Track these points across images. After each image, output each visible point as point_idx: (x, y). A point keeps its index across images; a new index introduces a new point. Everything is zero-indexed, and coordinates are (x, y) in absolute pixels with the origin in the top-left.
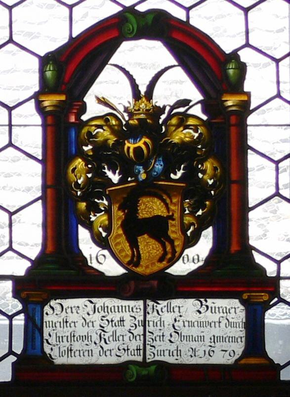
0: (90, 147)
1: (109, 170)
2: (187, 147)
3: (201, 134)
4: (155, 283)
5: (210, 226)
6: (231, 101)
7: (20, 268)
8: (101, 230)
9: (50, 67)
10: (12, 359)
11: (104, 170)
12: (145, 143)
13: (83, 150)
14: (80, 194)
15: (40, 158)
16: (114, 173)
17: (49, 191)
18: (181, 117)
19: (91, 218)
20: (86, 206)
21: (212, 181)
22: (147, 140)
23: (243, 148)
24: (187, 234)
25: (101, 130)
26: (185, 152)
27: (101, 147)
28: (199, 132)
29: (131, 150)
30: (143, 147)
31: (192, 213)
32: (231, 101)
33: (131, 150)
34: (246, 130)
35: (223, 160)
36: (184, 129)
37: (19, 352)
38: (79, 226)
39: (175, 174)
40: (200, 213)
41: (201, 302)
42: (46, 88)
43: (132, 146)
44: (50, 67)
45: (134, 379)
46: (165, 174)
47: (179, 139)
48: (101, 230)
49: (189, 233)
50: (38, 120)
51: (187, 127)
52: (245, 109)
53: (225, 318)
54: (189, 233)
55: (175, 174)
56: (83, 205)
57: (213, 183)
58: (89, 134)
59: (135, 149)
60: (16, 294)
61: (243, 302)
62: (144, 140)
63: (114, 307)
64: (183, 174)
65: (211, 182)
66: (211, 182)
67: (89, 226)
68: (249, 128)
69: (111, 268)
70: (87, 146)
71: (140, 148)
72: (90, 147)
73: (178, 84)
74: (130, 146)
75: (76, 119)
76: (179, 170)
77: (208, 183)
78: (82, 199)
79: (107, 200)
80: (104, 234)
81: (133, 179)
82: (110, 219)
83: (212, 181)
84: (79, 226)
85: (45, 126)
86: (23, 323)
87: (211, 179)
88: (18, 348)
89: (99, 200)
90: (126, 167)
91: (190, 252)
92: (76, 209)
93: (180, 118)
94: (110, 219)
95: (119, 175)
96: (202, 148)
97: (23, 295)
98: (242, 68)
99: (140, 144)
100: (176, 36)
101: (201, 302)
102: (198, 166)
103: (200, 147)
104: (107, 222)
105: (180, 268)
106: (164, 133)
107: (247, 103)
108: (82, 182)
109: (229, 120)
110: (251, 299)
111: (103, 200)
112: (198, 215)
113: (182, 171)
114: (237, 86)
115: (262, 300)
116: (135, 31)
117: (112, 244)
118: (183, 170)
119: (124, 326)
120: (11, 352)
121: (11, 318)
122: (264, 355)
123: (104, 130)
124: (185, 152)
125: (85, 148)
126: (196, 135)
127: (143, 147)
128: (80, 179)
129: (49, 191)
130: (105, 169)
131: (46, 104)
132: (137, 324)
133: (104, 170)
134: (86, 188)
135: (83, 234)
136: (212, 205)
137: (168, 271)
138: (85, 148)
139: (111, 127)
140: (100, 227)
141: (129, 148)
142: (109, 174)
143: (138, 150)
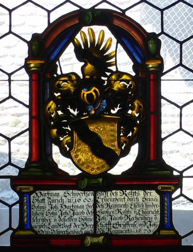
0: (59, 94)
1: (71, 108)
2: (123, 91)
3: (131, 85)
4: (101, 180)
5: (136, 143)
6: (151, 65)
7: (14, 172)
8: (66, 146)
9: (35, 42)
10: (11, 232)
11: (68, 108)
12: (95, 91)
13: (55, 96)
14: (53, 124)
15: (28, 104)
16: (74, 110)
17: (34, 120)
18: (118, 74)
19: (60, 139)
20: (57, 132)
21: (138, 114)
22: (97, 90)
23: (158, 97)
24: (122, 149)
25: (66, 83)
26: (120, 97)
27: (66, 93)
28: (130, 83)
29: (85, 95)
30: (94, 94)
31: (125, 135)
32: (151, 65)
33: (85, 95)
34: (160, 82)
35: (145, 100)
36: (120, 82)
37: (15, 228)
38: (53, 144)
39: (114, 110)
40: (130, 134)
41: (123, 192)
42: (32, 55)
43: (86, 93)
44: (35, 42)
45: (89, 244)
46: (108, 110)
47: (117, 88)
48: (66, 146)
49: (123, 148)
50: (27, 77)
51: (121, 81)
52: (159, 71)
53: (38, 196)
54: (123, 148)
55: (114, 110)
56: (55, 131)
57: (139, 116)
58: (59, 85)
59: (87, 95)
60: (14, 187)
61: (158, 192)
62: (94, 88)
63: (44, 194)
64: (119, 110)
65: (137, 115)
66: (137, 115)
67: (60, 144)
68: (162, 82)
69: (73, 171)
70: (57, 93)
71: (91, 94)
72: (59, 94)
73: (120, 53)
74: (85, 93)
75: (50, 76)
76: (116, 108)
77: (135, 116)
78: (54, 127)
79: (70, 127)
80: (68, 149)
81: (86, 113)
82: (72, 139)
83: (138, 114)
84: (53, 144)
85: (31, 81)
86: (18, 207)
87: (137, 113)
88: (15, 225)
89: (65, 127)
90: (82, 107)
91: (122, 161)
92: (50, 133)
93: (118, 75)
94: (72, 139)
95: (77, 111)
96: (131, 93)
97: (18, 188)
98: (158, 44)
99: (92, 91)
100: (117, 23)
101: (123, 192)
102: (129, 105)
103: (130, 93)
104: (70, 141)
105: (117, 170)
106: (105, 86)
107: (161, 66)
108: (54, 116)
109: (150, 77)
110: (21, 190)
111: (68, 127)
112: (129, 136)
113: (118, 108)
114: (157, 56)
115: (29, 191)
116: (91, 20)
117: (73, 155)
118: (119, 107)
119: (44, 202)
120: (10, 228)
121: (10, 206)
122: (172, 227)
123: (68, 83)
124: (120, 97)
125: (56, 95)
126: (128, 85)
127: (94, 94)
128: (53, 114)
129: (34, 120)
130: (68, 107)
131: (32, 65)
132: (51, 201)
133: (68, 108)
134: (56, 120)
135: (55, 149)
136: (138, 131)
137: (109, 172)
138: (56, 95)
139: (72, 81)
140: (66, 144)
141: (84, 94)
142: (72, 111)
143: (90, 96)
